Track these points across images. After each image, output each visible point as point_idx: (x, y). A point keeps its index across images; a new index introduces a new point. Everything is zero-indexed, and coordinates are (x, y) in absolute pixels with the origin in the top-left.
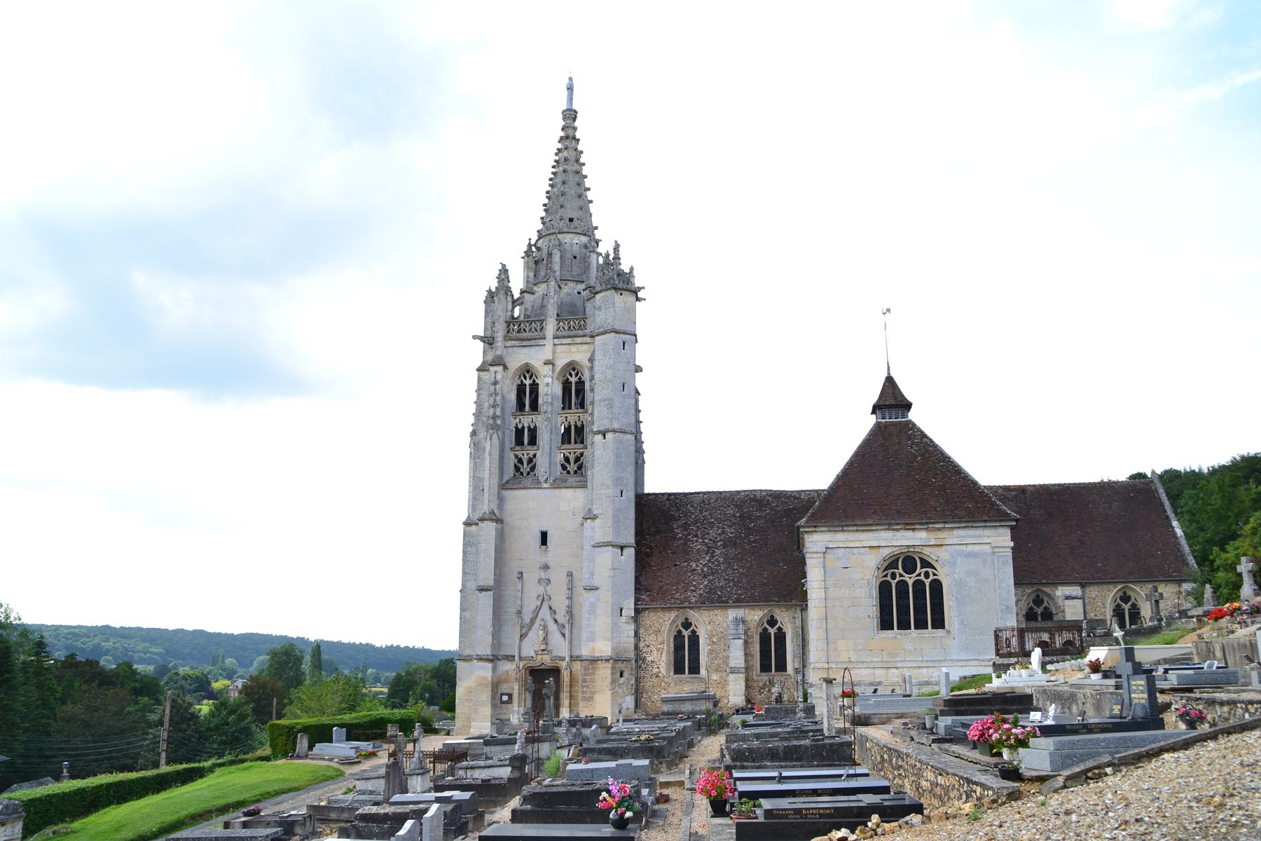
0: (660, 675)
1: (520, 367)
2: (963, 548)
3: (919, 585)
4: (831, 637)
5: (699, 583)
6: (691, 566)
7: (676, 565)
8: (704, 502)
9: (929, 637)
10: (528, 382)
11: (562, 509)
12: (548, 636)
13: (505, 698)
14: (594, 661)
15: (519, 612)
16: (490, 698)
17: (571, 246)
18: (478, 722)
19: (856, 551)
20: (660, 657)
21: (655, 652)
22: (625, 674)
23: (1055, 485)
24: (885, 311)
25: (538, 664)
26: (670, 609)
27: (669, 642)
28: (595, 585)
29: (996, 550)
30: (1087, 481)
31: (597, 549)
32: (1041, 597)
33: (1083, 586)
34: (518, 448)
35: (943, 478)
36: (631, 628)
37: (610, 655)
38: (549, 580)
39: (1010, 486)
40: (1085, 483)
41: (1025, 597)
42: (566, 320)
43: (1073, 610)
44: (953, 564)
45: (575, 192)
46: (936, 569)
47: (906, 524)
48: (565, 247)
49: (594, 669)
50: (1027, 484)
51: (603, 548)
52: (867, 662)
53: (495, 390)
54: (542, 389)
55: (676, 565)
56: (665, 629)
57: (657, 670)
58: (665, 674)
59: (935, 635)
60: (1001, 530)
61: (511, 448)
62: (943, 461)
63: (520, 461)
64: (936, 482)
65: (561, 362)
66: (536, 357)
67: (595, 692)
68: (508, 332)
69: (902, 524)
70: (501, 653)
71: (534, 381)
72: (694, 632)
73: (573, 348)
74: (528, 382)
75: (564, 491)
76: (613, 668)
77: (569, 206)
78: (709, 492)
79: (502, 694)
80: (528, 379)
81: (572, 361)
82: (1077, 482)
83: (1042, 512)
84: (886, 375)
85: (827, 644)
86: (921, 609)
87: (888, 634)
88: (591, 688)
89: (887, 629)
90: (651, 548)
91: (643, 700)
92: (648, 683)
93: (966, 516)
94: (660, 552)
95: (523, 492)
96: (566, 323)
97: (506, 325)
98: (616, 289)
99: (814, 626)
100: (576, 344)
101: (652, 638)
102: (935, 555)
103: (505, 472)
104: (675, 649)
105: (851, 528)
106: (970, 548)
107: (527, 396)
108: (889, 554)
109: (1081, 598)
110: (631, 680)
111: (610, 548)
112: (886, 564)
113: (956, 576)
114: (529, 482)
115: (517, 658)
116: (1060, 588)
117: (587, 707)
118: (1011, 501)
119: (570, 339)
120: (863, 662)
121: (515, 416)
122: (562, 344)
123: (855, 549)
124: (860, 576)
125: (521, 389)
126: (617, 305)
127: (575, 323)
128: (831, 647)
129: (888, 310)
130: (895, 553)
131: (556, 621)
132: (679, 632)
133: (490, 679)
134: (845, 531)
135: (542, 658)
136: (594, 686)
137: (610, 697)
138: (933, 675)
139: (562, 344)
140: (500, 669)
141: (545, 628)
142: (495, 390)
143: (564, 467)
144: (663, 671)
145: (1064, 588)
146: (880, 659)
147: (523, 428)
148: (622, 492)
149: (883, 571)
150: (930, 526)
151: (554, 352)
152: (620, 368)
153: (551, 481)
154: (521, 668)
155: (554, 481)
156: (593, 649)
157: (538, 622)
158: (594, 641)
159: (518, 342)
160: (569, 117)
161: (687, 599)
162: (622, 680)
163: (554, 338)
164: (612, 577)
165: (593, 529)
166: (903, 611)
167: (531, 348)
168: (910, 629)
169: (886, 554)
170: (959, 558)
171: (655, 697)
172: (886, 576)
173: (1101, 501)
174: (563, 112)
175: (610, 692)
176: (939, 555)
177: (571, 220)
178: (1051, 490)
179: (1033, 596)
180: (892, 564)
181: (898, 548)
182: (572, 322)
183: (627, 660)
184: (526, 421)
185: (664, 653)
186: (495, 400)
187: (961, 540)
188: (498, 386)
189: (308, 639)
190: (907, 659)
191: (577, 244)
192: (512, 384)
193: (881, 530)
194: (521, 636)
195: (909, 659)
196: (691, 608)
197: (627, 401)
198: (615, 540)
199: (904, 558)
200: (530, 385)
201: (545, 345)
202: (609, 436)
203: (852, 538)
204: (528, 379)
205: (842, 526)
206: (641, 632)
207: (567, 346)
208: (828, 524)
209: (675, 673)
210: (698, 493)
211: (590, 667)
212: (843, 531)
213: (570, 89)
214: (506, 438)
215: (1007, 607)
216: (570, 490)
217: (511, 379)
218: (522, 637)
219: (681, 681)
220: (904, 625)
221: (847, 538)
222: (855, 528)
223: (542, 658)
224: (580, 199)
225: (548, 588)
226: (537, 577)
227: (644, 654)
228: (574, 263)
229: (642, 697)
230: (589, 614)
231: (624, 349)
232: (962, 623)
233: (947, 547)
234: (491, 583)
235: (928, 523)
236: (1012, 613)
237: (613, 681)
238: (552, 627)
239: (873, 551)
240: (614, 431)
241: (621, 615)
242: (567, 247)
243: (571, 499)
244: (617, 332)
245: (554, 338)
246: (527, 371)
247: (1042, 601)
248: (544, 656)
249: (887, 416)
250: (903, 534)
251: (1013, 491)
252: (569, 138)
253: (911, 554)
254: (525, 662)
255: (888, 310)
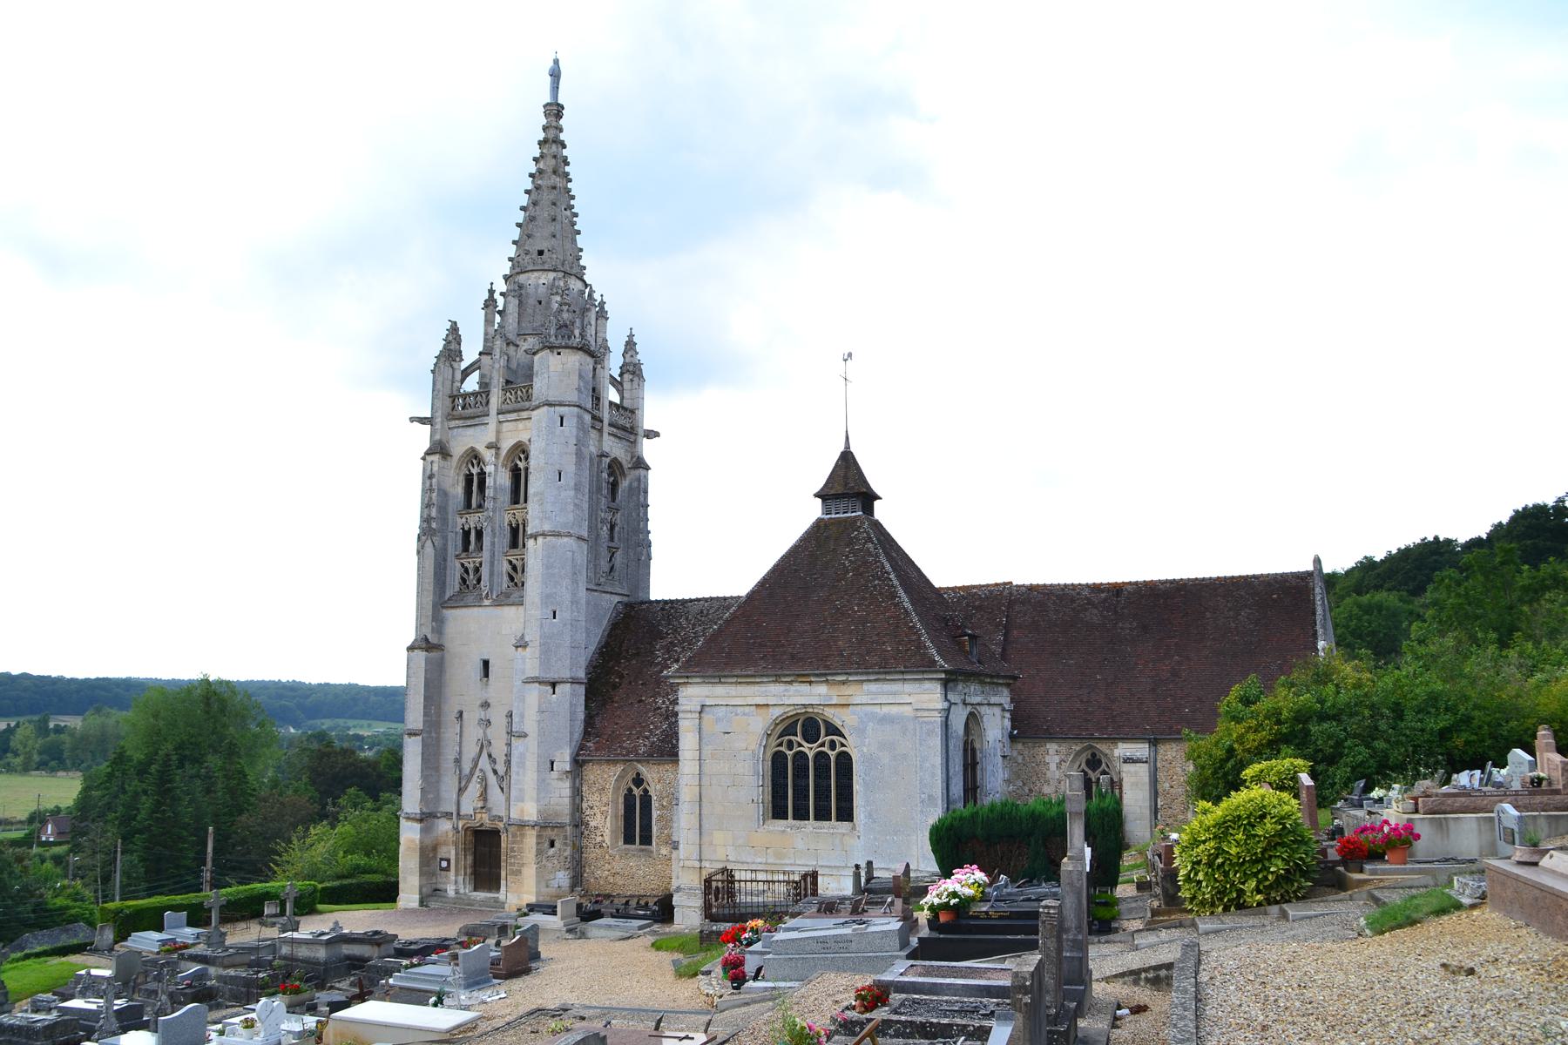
0: (604, 845)
1: (465, 453)
2: (877, 709)
3: (820, 756)
4: (706, 826)
5: (656, 728)
6: (656, 703)
7: (640, 701)
8: (702, 612)
9: (826, 833)
10: (475, 471)
11: (504, 632)
12: (488, 791)
13: (444, 864)
14: (522, 825)
15: (458, 761)
16: (418, 866)
17: (535, 288)
18: (407, 893)
19: (740, 710)
20: (604, 821)
21: (599, 815)
22: (556, 844)
23: (1167, 581)
24: (846, 357)
25: (478, 825)
26: (615, 762)
27: (617, 803)
28: (525, 731)
29: (919, 714)
30: (1214, 575)
31: (527, 685)
32: (1098, 757)
33: (1154, 743)
34: (464, 555)
35: (870, 604)
36: (565, 788)
37: (535, 819)
38: (489, 721)
39: (1101, 584)
40: (1211, 578)
41: (1071, 757)
42: (524, 387)
43: (1133, 779)
44: (861, 731)
45: (549, 215)
46: (845, 738)
47: (798, 675)
48: (529, 291)
49: (523, 835)
50: (1127, 580)
51: (531, 684)
52: (748, 863)
53: (431, 485)
54: (489, 481)
55: (640, 701)
56: (610, 787)
57: (601, 838)
58: (609, 844)
59: (835, 831)
60: (927, 685)
61: (457, 556)
62: (879, 579)
63: (466, 571)
64: (858, 611)
65: (506, 445)
66: (477, 438)
67: (523, 865)
68: (453, 408)
69: (793, 675)
70: (441, 809)
71: (482, 469)
72: (646, 791)
73: (521, 425)
74: (475, 471)
75: (506, 609)
76: (539, 837)
77: (539, 234)
78: (712, 599)
79: (442, 859)
80: (476, 467)
81: (520, 442)
82: (1200, 576)
83: (1135, 624)
84: (842, 449)
85: (700, 834)
86: (822, 794)
87: (780, 824)
88: (518, 859)
89: (781, 819)
90: (621, 677)
91: (585, 875)
92: (591, 854)
93: (875, 665)
94: (630, 683)
95: (464, 610)
96: (513, 392)
97: (451, 399)
98: (551, 348)
99: (685, 812)
100: (524, 419)
101: (595, 798)
102: (840, 719)
103: (448, 587)
104: (625, 812)
105: (730, 680)
106: (885, 709)
107: (475, 484)
108: (780, 716)
109: (1146, 762)
110: (565, 850)
111: (537, 685)
112: (780, 728)
113: (865, 750)
114: (473, 597)
115: (454, 816)
116: (1121, 745)
117: (515, 883)
118: (1096, 608)
119: (516, 414)
120: (742, 863)
121: (461, 515)
122: (508, 421)
123: (739, 708)
124: (744, 745)
125: (469, 479)
126: (552, 369)
127: (522, 392)
128: (705, 839)
129: (850, 355)
130: (789, 715)
131: (495, 772)
132: (630, 790)
133: (418, 842)
134: (725, 683)
135: (481, 818)
136: (522, 857)
137: (534, 873)
138: (830, 886)
139: (508, 421)
140: (440, 827)
141: (484, 779)
142: (431, 485)
143: (512, 579)
144: (607, 840)
145: (1125, 745)
146: (764, 860)
147: (470, 529)
148: (555, 613)
149: (778, 738)
150: (829, 678)
151: (498, 432)
152: (555, 452)
153: (494, 597)
154: (460, 829)
155: (497, 597)
156: (522, 811)
157: (477, 773)
158: (523, 801)
159: (461, 422)
160: (549, 114)
161: (635, 750)
162: (552, 851)
163: (498, 414)
164: (539, 721)
165: (524, 659)
166: (801, 794)
167: (476, 427)
168: (809, 820)
169: (777, 715)
170: (871, 724)
171: (599, 872)
172: (781, 745)
173: (1226, 606)
174: (545, 106)
175: (535, 866)
176: (844, 718)
177: (541, 253)
178: (1159, 589)
179: (1084, 758)
180: (789, 730)
181: (792, 708)
182: (519, 392)
183: (561, 826)
184: (473, 520)
185: (609, 817)
186: (431, 498)
187: (872, 699)
188: (434, 480)
189: (1436, 538)
190: (798, 862)
191: (544, 284)
192: (458, 474)
193: (769, 682)
194: (460, 790)
195: (800, 863)
196: (638, 761)
197: (563, 494)
198: (543, 675)
199: (804, 721)
200: (479, 474)
201: (487, 424)
202: (540, 539)
203: (734, 693)
204: (476, 467)
205: (720, 677)
206: (584, 789)
207: (513, 423)
208: (701, 674)
209: (625, 843)
210: (698, 600)
211: (518, 833)
212: (720, 682)
213: (555, 75)
214: (449, 543)
215: (929, 796)
216: (513, 608)
217: (456, 468)
218: (461, 791)
219: (627, 854)
220: (801, 815)
221: (728, 693)
222: (734, 680)
223: (481, 818)
224: (554, 223)
225: (489, 731)
226: (477, 717)
227: (588, 818)
228: (537, 310)
229: (585, 871)
230: (518, 767)
231: (562, 425)
232: (870, 816)
233: (854, 707)
234: (420, 726)
235: (825, 675)
236: (936, 805)
237: (539, 853)
238: (492, 779)
239: (763, 711)
240: (544, 535)
241: (552, 770)
242: (531, 290)
243: (510, 620)
244: (550, 405)
245: (498, 414)
246: (474, 456)
247: (1100, 762)
248: (483, 815)
249: (833, 512)
250: (798, 688)
251: (1103, 592)
252: (552, 141)
253: (812, 716)
254: (465, 822)
255: (850, 355)
